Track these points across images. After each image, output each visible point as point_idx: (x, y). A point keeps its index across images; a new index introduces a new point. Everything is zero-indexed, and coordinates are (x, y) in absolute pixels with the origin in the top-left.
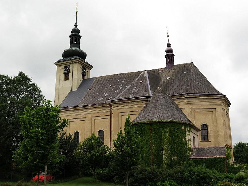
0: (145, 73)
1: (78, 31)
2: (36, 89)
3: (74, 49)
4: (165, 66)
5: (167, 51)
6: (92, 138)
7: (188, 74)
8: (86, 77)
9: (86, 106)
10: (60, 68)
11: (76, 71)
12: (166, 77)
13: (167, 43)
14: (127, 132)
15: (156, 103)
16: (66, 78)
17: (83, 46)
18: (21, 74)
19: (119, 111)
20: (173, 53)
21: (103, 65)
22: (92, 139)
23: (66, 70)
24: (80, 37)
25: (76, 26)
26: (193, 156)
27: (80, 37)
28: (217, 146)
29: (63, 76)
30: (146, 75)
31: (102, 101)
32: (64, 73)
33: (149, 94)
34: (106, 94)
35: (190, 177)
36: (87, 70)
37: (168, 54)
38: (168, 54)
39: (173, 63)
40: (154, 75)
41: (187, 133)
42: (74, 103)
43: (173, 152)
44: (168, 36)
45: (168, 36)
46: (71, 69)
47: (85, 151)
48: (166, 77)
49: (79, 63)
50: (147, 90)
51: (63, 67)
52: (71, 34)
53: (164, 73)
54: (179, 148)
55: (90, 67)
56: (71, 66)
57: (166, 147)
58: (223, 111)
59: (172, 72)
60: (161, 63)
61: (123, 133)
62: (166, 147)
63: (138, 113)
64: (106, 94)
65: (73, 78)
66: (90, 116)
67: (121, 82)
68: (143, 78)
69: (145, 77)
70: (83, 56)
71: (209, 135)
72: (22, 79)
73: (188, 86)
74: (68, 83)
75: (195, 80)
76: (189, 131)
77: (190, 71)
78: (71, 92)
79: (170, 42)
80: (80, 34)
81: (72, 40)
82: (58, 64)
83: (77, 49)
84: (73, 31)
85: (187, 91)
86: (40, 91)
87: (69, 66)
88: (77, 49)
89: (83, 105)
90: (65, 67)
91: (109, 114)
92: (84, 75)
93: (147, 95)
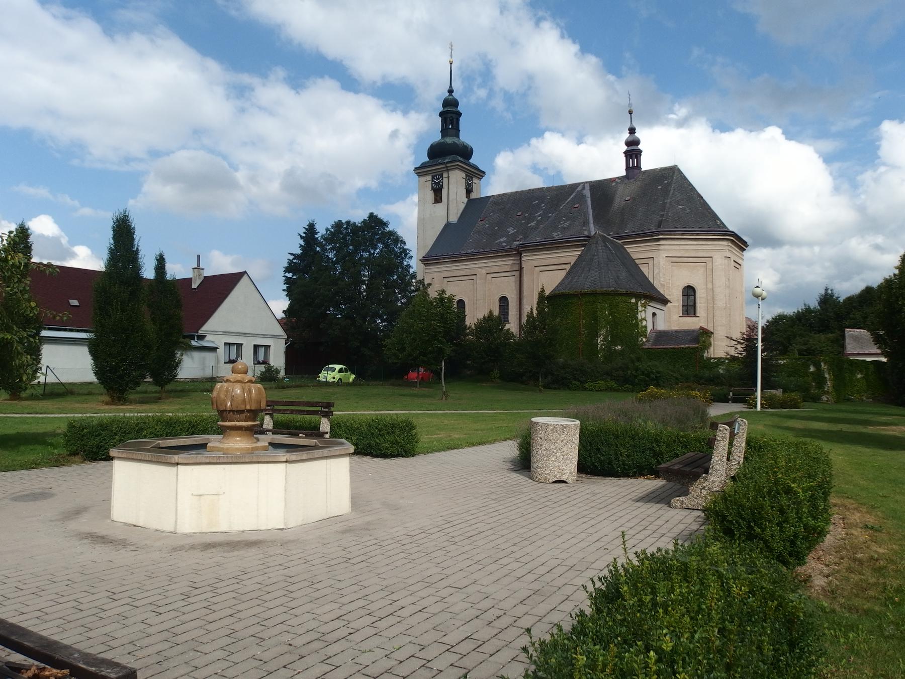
0: (584, 188)
1: (455, 103)
2: (397, 240)
3: (449, 140)
4: (624, 174)
5: (628, 143)
6: (489, 317)
8: (473, 196)
9: (473, 254)
10: (424, 179)
11: (455, 182)
12: (622, 196)
14: (539, 313)
15: (592, 260)
16: (438, 199)
17: (467, 135)
18: (371, 215)
19: (536, 263)
20: (640, 147)
21: (507, 172)
22: (490, 318)
23: (436, 183)
24: (460, 114)
25: (451, 91)
27: (460, 114)
29: (430, 195)
30: (587, 193)
31: (504, 244)
32: (433, 189)
33: (589, 231)
34: (511, 231)
35: (636, 376)
36: (475, 180)
37: (631, 148)
38: (631, 148)
39: (638, 167)
40: (601, 190)
41: (640, 309)
42: (450, 246)
43: (615, 338)
44: (630, 113)
45: (630, 113)
46: (445, 181)
47: (478, 338)
48: (622, 196)
49: (462, 169)
50: (586, 223)
51: (429, 178)
52: (441, 109)
53: (621, 188)
54: (626, 328)
55: (480, 174)
56: (445, 175)
57: (603, 331)
58: (726, 261)
59: (633, 187)
60: (617, 168)
61: (535, 312)
62: (603, 331)
63: (568, 267)
64: (511, 231)
65: (450, 199)
66: (484, 271)
68: (581, 197)
69: (584, 196)
70: (466, 152)
71: (698, 305)
72: (374, 223)
73: (662, 216)
74: (441, 208)
75: (678, 203)
76: (644, 306)
77: (669, 184)
78: (448, 226)
81: (444, 122)
82: (421, 170)
83: (456, 140)
85: (659, 227)
86: (404, 243)
87: (442, 176)
88: (456, 140)
89: (469, 251)
90: (433, 178)
91: (517, 267)
92: (469, 191)
93: (586, 233)
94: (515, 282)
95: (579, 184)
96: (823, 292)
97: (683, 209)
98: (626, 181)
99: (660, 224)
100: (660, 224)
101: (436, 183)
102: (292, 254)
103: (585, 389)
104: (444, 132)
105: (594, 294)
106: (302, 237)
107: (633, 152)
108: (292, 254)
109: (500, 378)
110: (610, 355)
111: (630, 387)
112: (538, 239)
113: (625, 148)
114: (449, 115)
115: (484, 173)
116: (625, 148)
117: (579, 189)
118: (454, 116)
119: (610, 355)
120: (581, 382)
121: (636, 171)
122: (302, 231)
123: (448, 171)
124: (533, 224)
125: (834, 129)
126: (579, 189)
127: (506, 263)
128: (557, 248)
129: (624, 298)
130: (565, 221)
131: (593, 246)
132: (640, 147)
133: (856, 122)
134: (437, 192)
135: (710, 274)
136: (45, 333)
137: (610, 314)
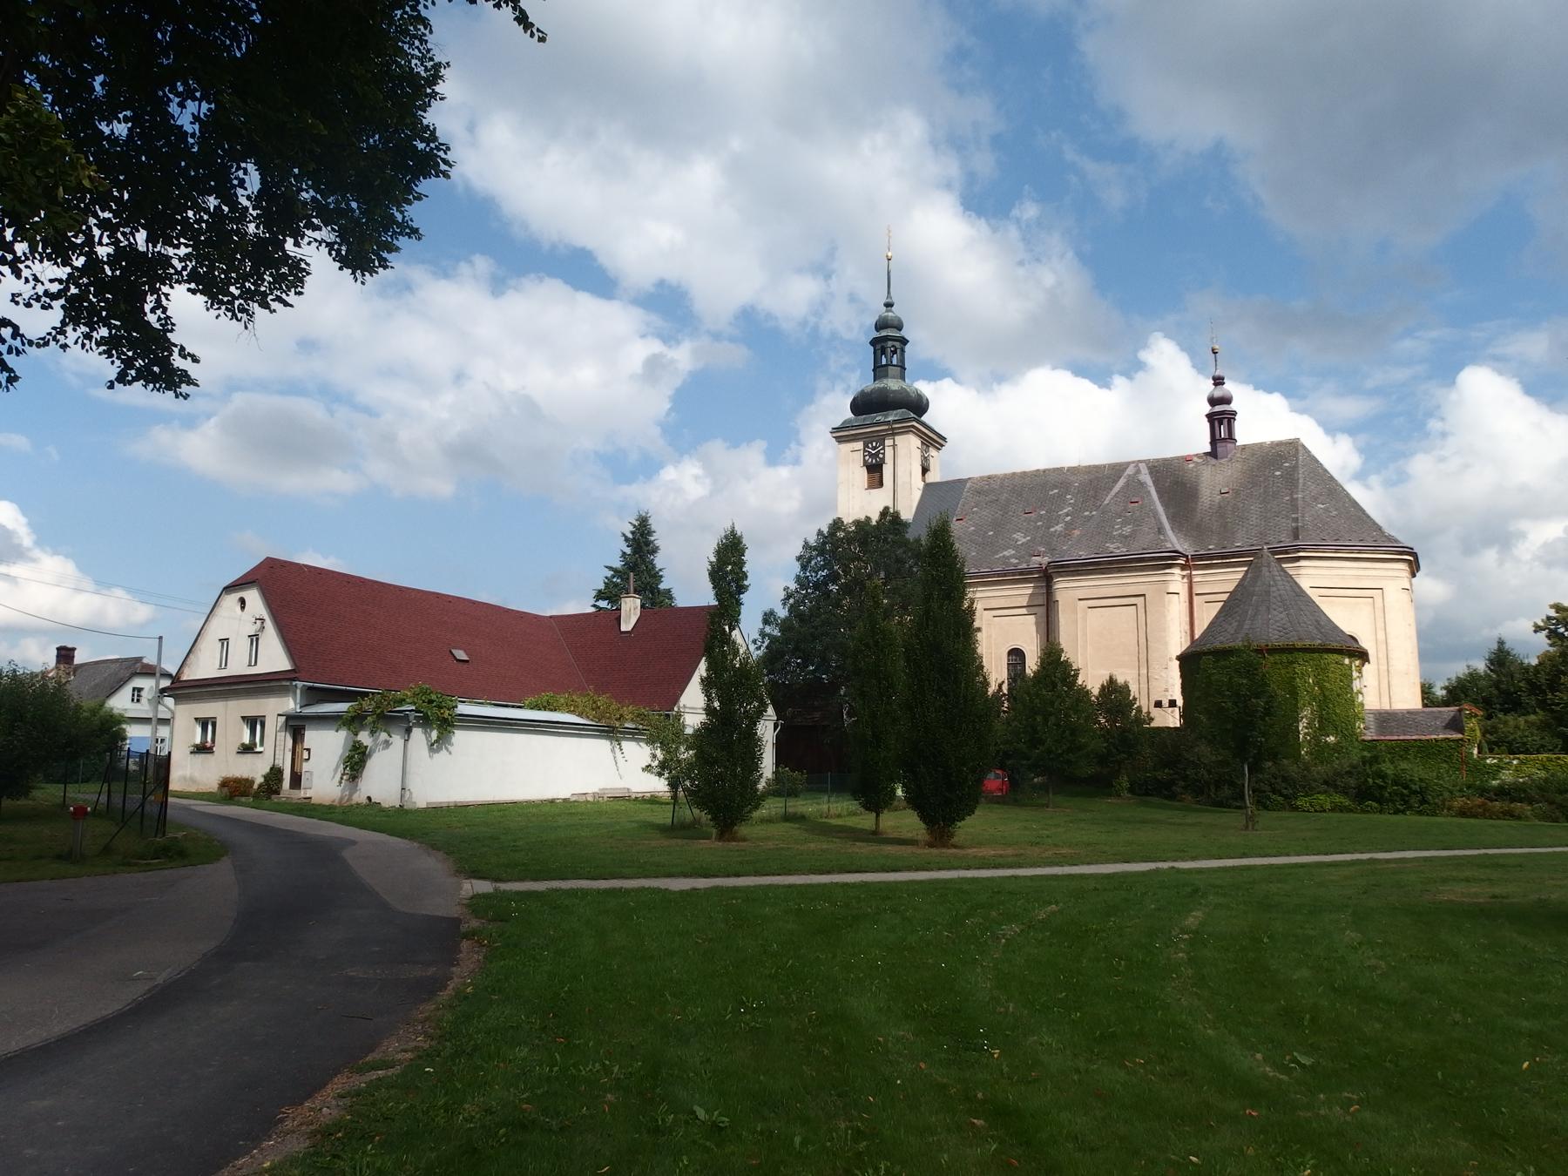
0: (1138, 472)
4: (1208, 449)
5: (1213, 401)
7: (1290, 479)
12: (1213, 483)
13: (884, 300)
20: (1233, 406)
23: (871, 455)
25: (889, 305)
26: (1369, 736)
28: (1386, 707)
30: (1146, 478)
31: (1014, 561)
32: (865, 464)
35: (1381, 788)
38: (1218, 408)
39: (1231, 437)
40: (1173, 480)
41: (1355, 674)
43: (1325, 722)
46: (889, 452)
51: (860, 445)
56: (888, 442)
62: (1307, 712)
64: (1021, 538)
65: (899, 481)
67: (1061, 496)
69: (1142, 484)
73: (1296, 520)
75: (1315, 499)
77: (1295, 468)
79: (895, 299)
80: (904, 333)
84: (881, 325)
85: (1296, 537)
90: (866, 446)
94: (1037, 624)
95: (1128, 464)
96: (1495, 646)
97: (1326, 510)
98: (1213, 461)
99: (1296, 534)
100: (1296, 534)
101: (871, 455)
102: (610, 568)
103: (1296, 809)
104: (879, 371)
105: (1290, 650)
106: (627, 539)
107: (1221, 418)
108: (610, 568)
109: (1131, 790)
110: (1320, 750)
111: (1375, 804)
112: (1083, 554)
113: (1207, 409)
114: (890, 343)
115: (944, 439)
116: (1207, 409)
117: (1130, 471)
118: (897, 344)
119: (1320, 750)
120: (1286, 797)
121: (1230, 446)
122: (628, 530)
123: (894, 434)
124: (1059, 528)
125: (1370, 384)
126: (1130, 471)
127: (1022, 593)
128: (1120, 570)
129: (1335, 656)
130: (1124, 524)
131: (1265, 569)
132: (1233, 406)
133: (1400, 374)
134: (875, 470)
135: (1381, 617)
136: (464, 709)
137: (1317, 683)
